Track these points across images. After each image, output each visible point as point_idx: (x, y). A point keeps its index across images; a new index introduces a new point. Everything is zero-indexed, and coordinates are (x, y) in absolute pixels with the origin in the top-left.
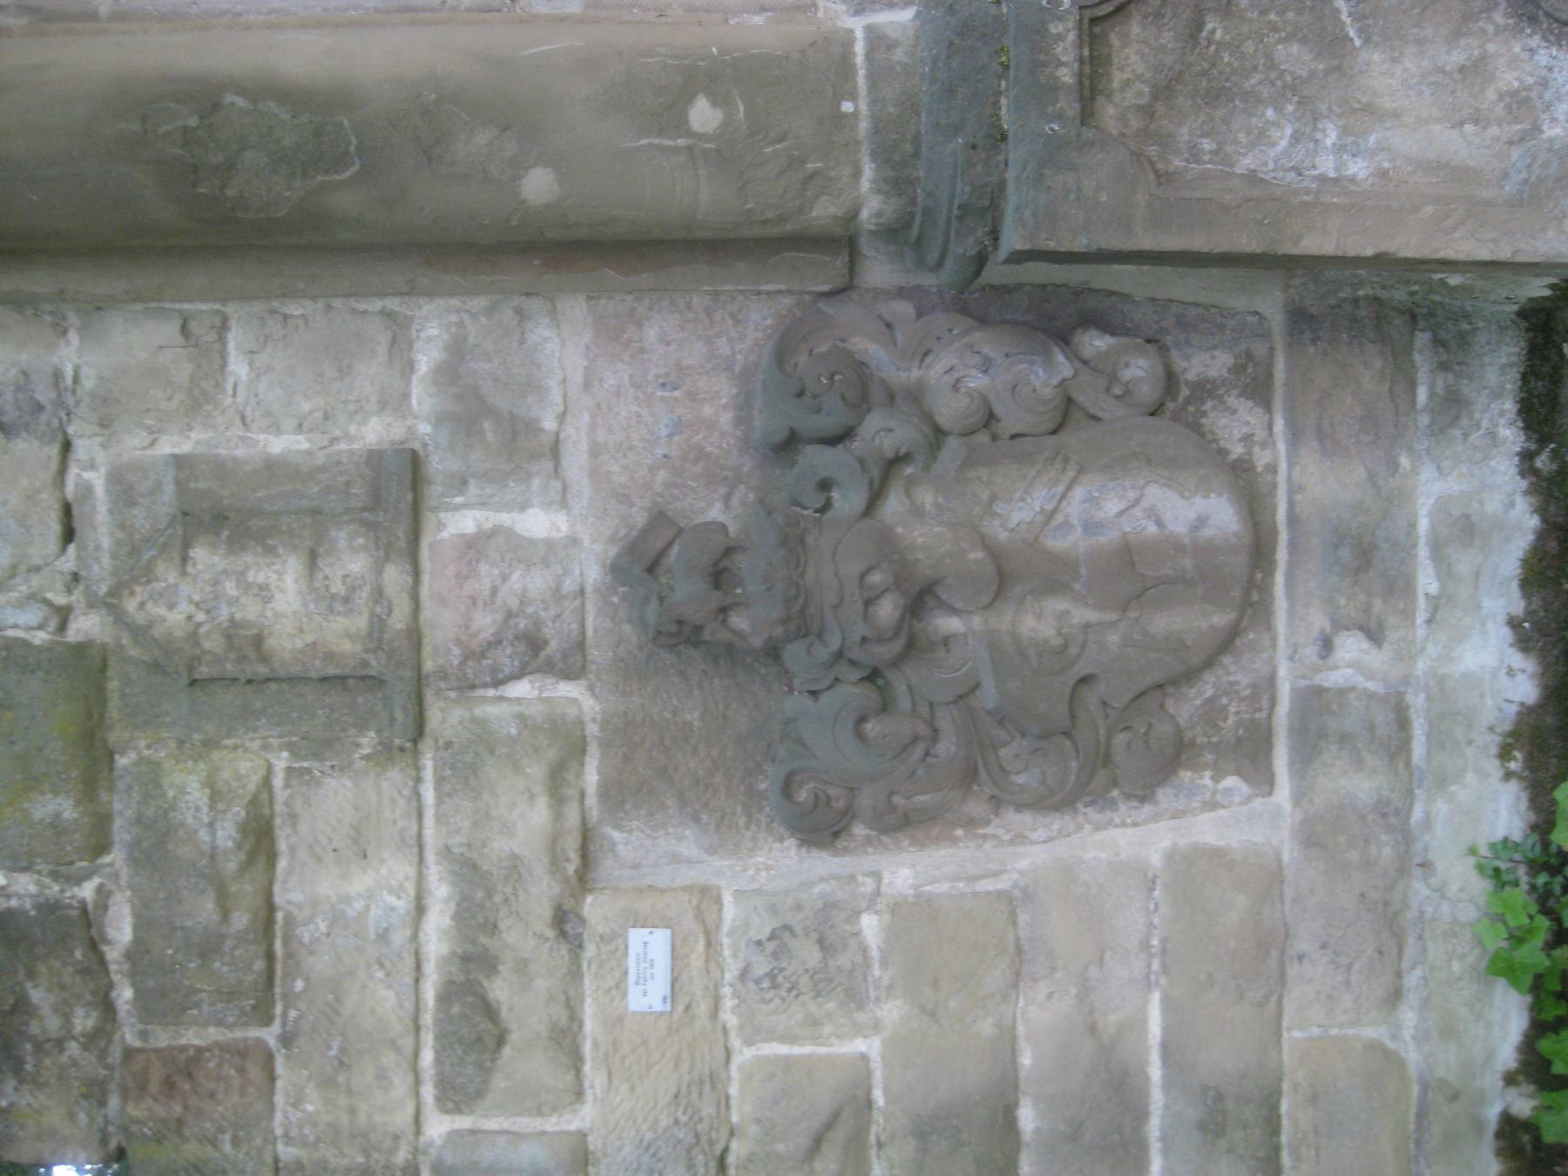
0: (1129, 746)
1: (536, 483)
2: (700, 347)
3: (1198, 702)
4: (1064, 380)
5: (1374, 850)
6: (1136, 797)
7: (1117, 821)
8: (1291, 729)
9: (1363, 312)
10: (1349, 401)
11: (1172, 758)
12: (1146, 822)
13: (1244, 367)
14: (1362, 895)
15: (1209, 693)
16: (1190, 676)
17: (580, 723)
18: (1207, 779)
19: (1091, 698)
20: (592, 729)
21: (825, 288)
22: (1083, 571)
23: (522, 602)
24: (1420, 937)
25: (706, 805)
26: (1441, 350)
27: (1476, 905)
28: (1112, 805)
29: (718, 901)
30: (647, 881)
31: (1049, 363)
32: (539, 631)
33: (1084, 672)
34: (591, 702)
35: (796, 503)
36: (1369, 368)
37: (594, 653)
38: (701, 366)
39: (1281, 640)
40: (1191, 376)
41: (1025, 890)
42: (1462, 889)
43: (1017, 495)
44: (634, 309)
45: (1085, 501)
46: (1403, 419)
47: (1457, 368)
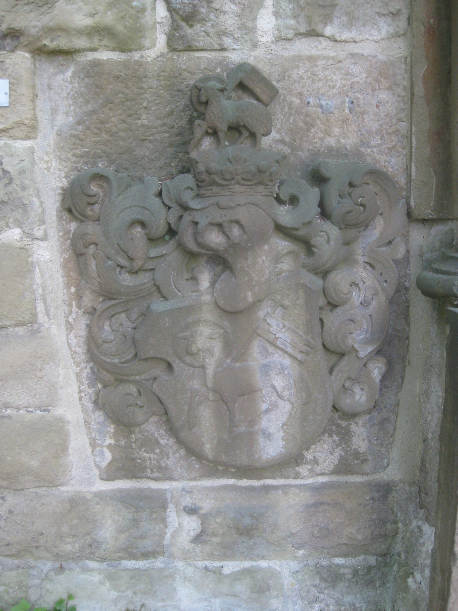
0: (129, 394)
1: (292, 22)
2: (375, 126)
3: (156, 435)
4: (357, 351)
5: (69, 540)
6: (97, 399)
7: (82, 388)
8: (140, 490)
9: (389, 526)
10: (338, 520)
11: (122, 421)
12: (82, 404)
13: (357, 459)
14: (42, 534)
15: (162, 442)
16: (172, 430)
17: (140, 48)
18: (109, 441)
19: (158, 370)
20: (136, 56)
21: (412, 204)
22: (238, 365)
23: (217, 10)
24: (18, 567)
25: (88, 128)
26: (365, 571)
27: (39, 599)
28: (92, 384)
29: (28, 138)
30: (40, 94)
31: (367, 342)
32: (199, 21)
33: (175, 366)
34: (153, 55)
35: (282, 183)
36: (356, 532)
37: (185, 56)
38: (364, 127)
39: (195, 483)
40: (353, 427)
41: (38, 331)
42: (48, 590)
43: (286, 323)
44: (398, 85)
45: (281, 365)
46: (326, 551)
47: (354, 580)
